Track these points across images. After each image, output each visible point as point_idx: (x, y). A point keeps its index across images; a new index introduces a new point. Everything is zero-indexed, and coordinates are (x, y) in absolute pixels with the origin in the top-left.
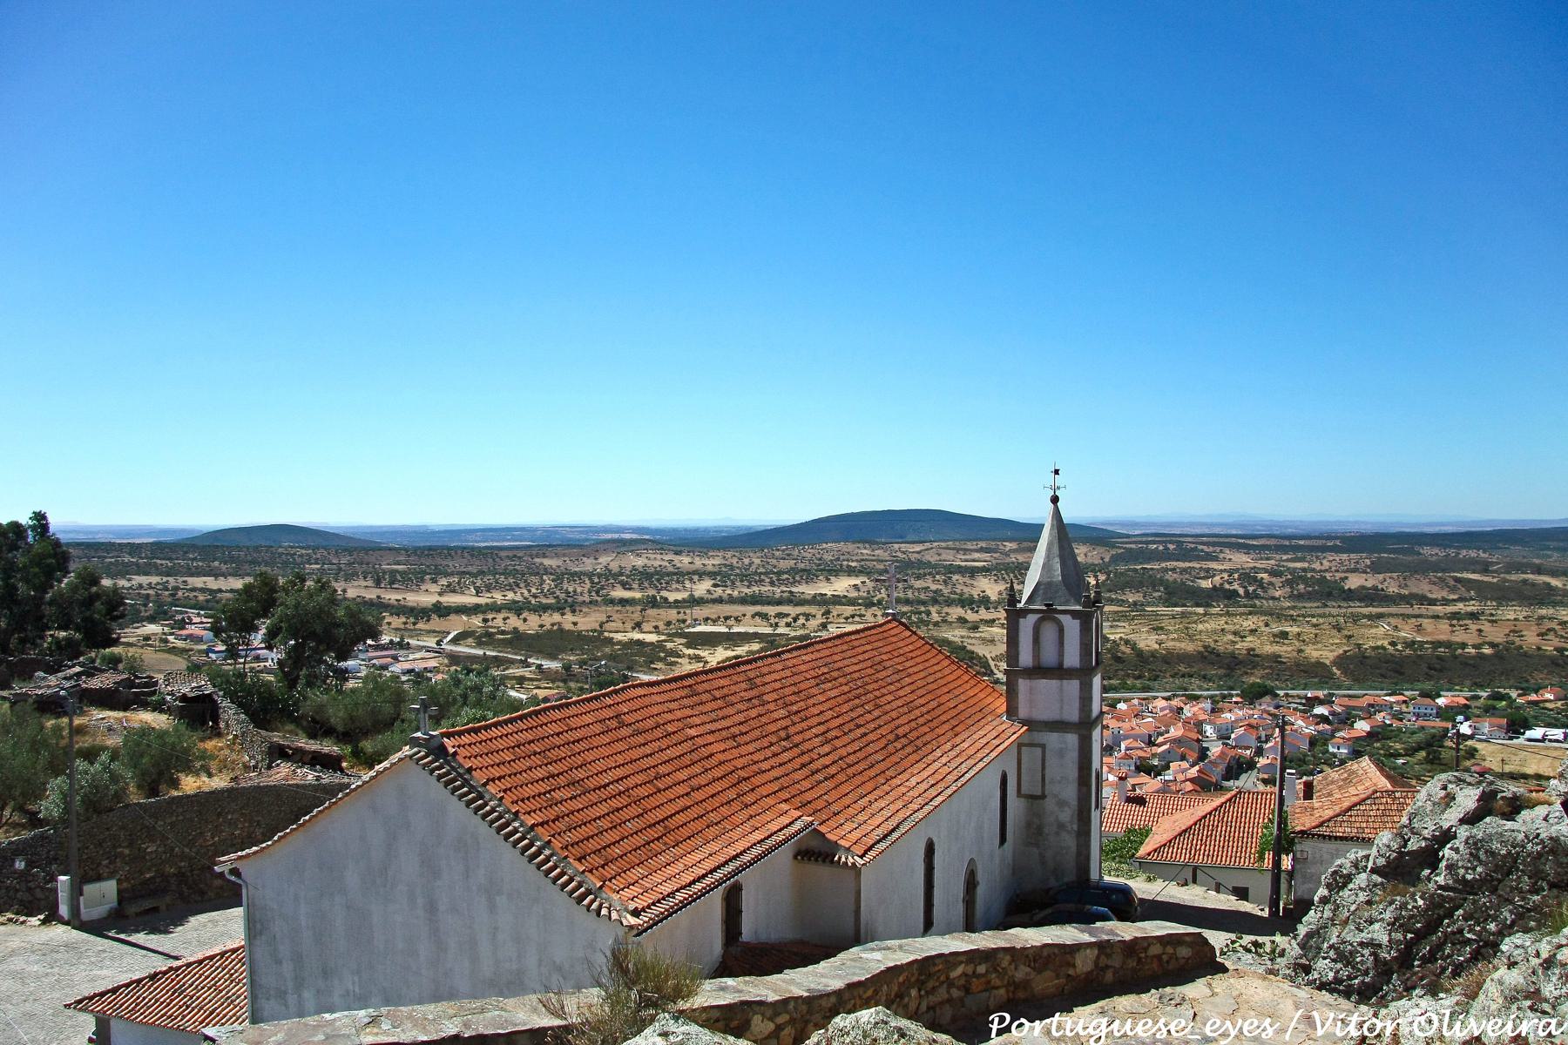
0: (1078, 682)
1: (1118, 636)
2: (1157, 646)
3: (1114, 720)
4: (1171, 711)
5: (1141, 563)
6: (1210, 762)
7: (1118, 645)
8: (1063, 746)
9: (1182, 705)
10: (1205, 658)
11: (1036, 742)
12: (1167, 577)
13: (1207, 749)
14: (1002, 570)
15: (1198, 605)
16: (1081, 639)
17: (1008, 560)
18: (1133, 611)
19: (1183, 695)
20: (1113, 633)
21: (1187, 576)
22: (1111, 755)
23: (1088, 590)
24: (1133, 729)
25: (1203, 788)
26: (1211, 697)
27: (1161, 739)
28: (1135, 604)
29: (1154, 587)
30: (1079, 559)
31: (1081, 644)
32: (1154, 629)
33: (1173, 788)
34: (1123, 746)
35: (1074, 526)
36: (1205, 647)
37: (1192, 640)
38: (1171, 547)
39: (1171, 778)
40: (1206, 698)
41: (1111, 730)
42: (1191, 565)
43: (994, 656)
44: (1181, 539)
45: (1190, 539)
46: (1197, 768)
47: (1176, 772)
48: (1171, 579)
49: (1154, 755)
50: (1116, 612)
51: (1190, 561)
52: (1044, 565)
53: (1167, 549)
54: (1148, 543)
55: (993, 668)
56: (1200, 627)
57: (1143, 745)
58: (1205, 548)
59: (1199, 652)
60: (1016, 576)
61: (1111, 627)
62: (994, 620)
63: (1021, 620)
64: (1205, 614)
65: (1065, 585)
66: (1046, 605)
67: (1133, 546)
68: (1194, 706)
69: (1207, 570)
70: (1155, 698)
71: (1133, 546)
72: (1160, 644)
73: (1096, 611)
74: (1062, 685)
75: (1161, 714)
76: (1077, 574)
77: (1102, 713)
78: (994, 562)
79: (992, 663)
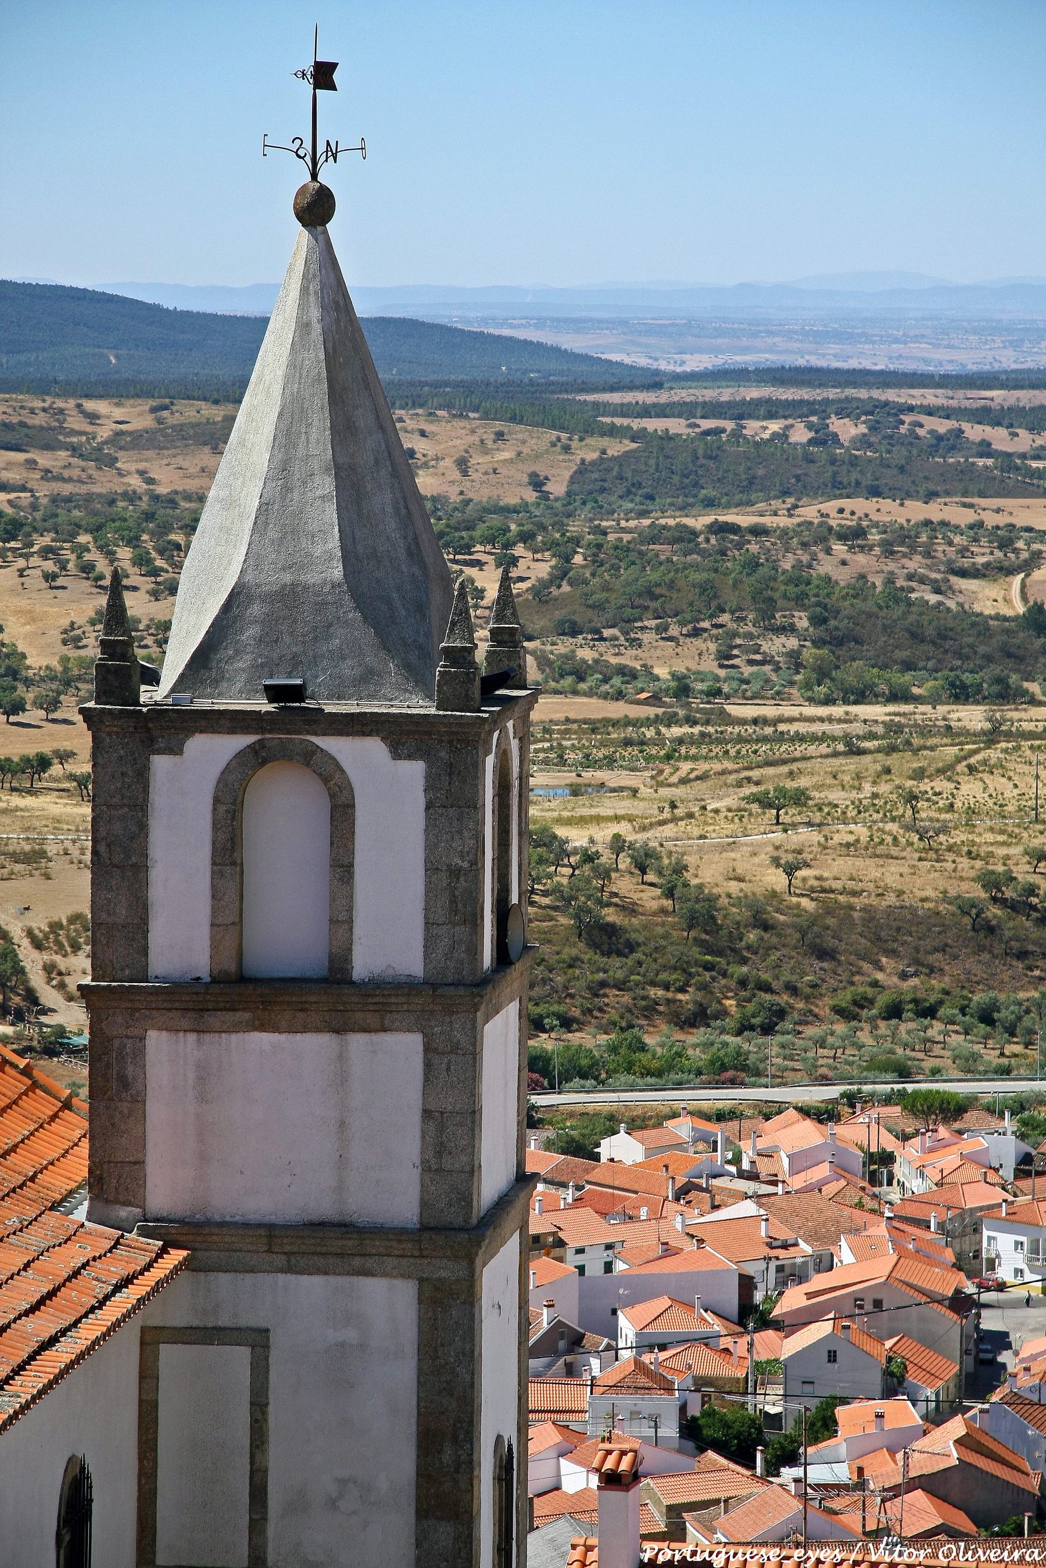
0: (413, 1042)
1: (604, 834)
2: (777, 880)
3: (587, 1213)
4: (841, 1169)
5: (710, 504)
6: (1015, 1400)
7: (605, 874)
8: (351, 1335)
9: (890, 1143)
10: (991, 930)
11: (224, 1321)
12: (826, 567)
13: (1001, 1340)
14: (77, 527)
15: (961, 694)
16: (430, 848)
17: (104, 483)
18: (671, 720)
19: (888, 1100)
20: (583, 821)
21: (915, 564)
22: (571, 1371)
23: (464, 623)
24: (668, 1251)
25: (982, 1521)
26: (1019, 1106)
27: (794, 1299)
28: (682, 689)
29: (766, 608)
30: (426, 483)
31: (431, 869)
32: (764, 802)
33: (852, 1520)
34: (627, 1327)
35: (383, 323)
36: (992, 882)
37: (932, 853)
38: (847, 430)
39: (842, 1473)
40: (994, 1110)
41: (572, 1260)
42: (935, 511)
43: (39, 923)
44: (891, 395)
45: (930, 397)
46: (956, 1427)
47: (860, 1452)
48: (843, 577)
49: (764, 1372)
50: (595, 726)
51: (930, 496)
52: (264, 508)
53: (824, 439)
54: (742, 411)
55: (37, 980)
56: (970, 790)
57: (717, 1326)
58: (999, 437)
59: (966, 907)
60: (142, 561)
61: (576, 791)
62: (43, 763)
63: (161, 764)
64: (992, 736)
65: (361, 602)
66: (274, 693)
67: (676, 426)
68: (941, 1145)
69: (1005, 536)
70: (769, 1111)
71: (676, 426)
72: (790, 870)
73: (496, 721)
74: (342, 1057)
75: (797, 1182)
76: (414, 553)
77: (524, 1180)
78: (44, 491)
79: (31, 960)
